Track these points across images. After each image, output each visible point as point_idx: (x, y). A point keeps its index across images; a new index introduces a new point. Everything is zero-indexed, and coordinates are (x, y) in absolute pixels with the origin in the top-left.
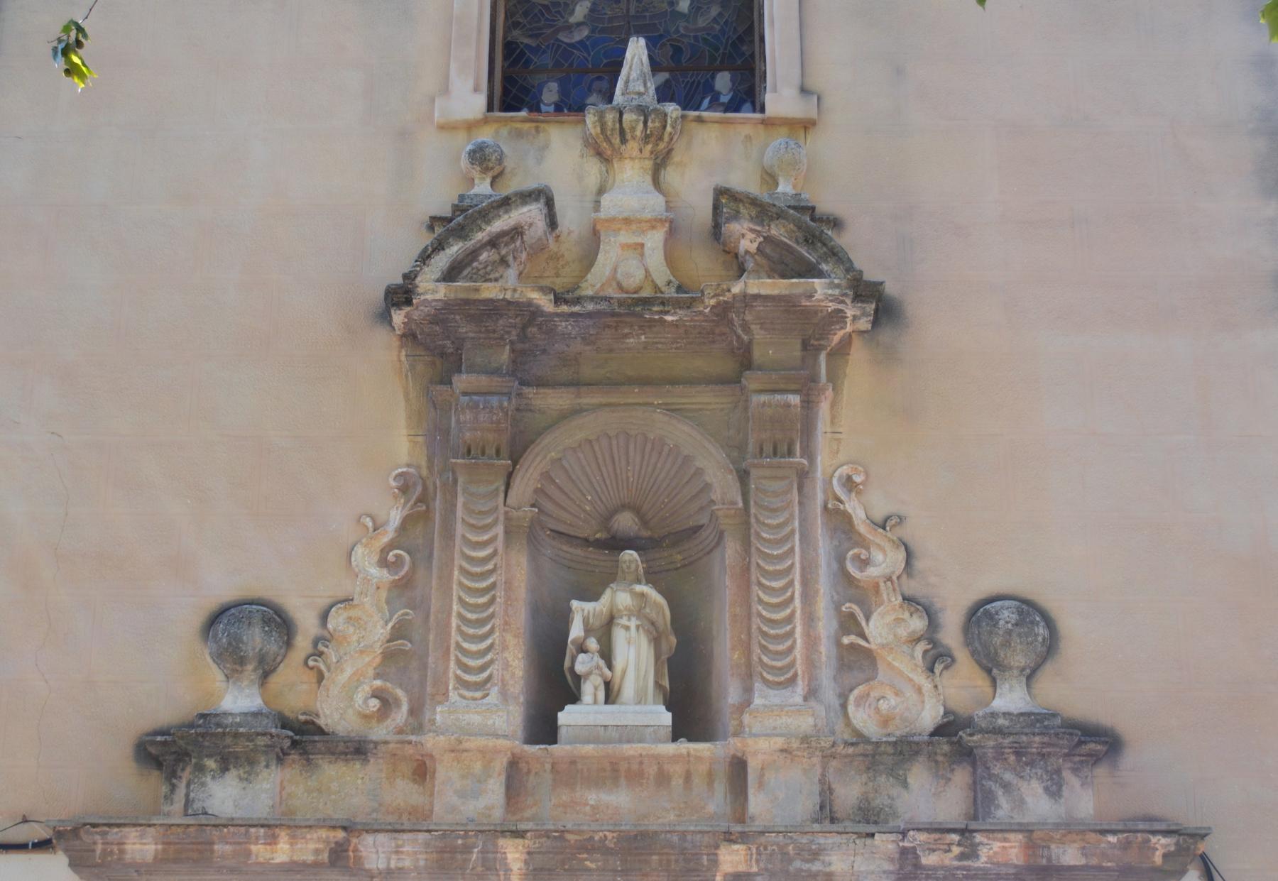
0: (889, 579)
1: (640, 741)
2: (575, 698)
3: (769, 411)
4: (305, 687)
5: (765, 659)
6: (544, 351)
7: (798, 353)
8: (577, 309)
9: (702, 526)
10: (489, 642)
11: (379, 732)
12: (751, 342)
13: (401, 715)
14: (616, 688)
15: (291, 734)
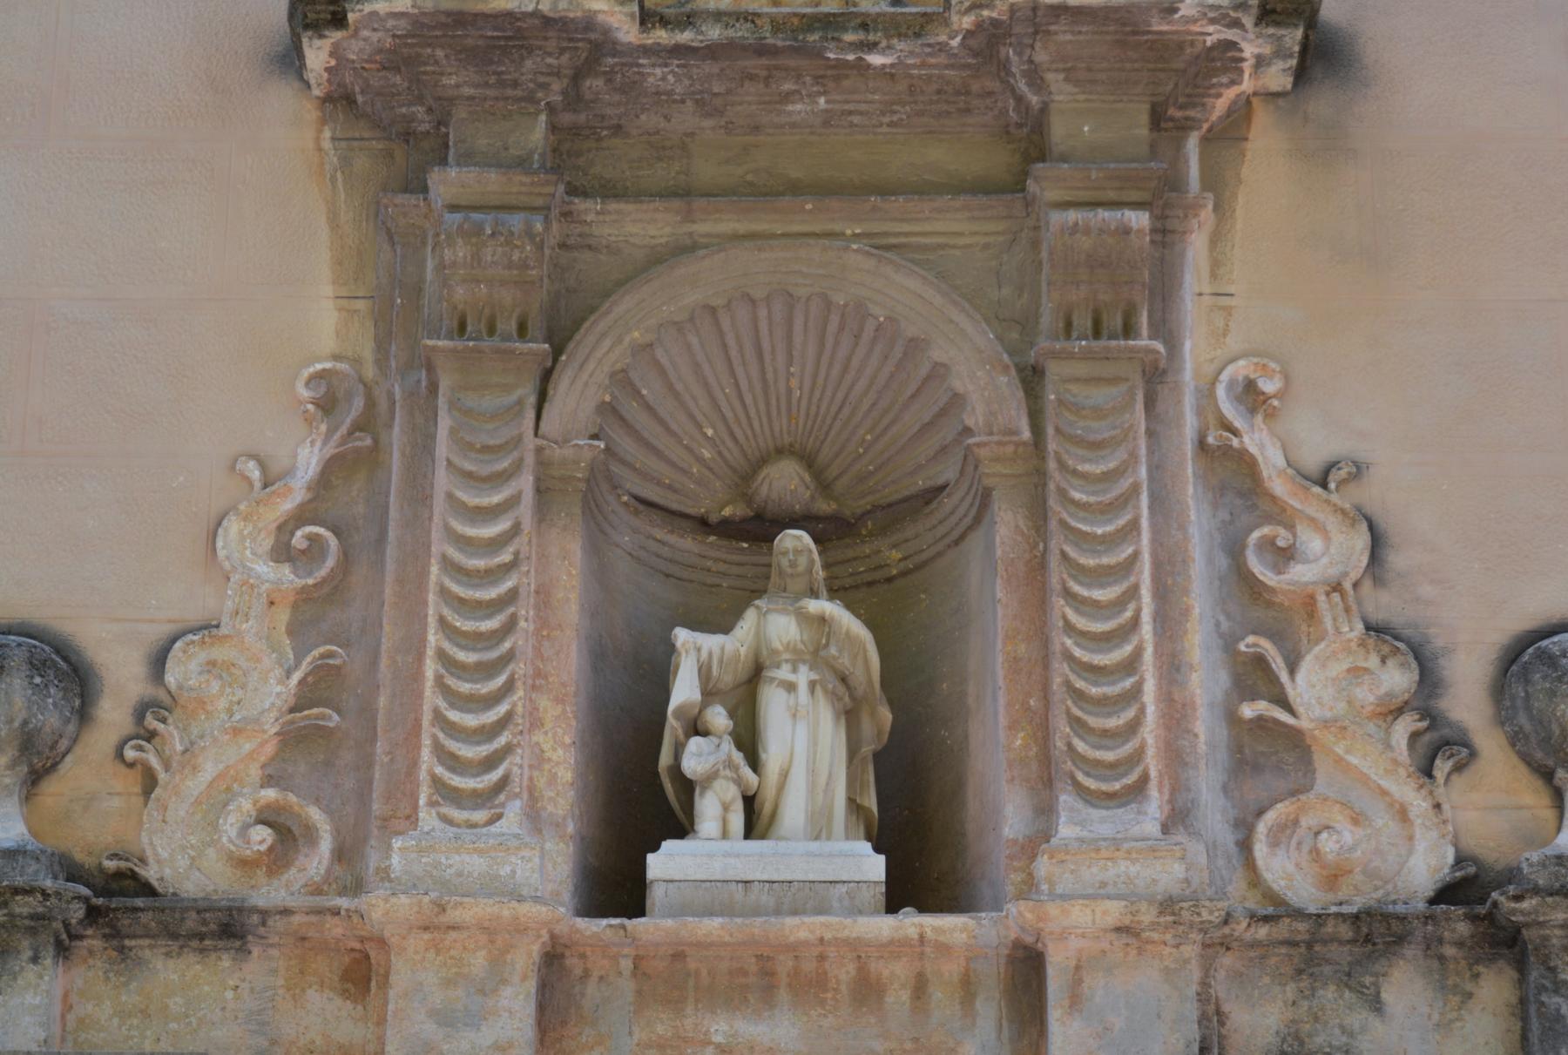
0: (1337, 587)
1: (821, 910)
2: (682, 829)
3: (1085, 243)
4: (116, 802)
5: (1080, 746)
6: (618, 130)
7: (1144, 132)
8: (686, 37)
9: (942, 488)
10: (502, 709)
11: (268, 893)
12: (1044, 109)
13: (317, 861)
14: (767, 809)
15: (84, 891)
